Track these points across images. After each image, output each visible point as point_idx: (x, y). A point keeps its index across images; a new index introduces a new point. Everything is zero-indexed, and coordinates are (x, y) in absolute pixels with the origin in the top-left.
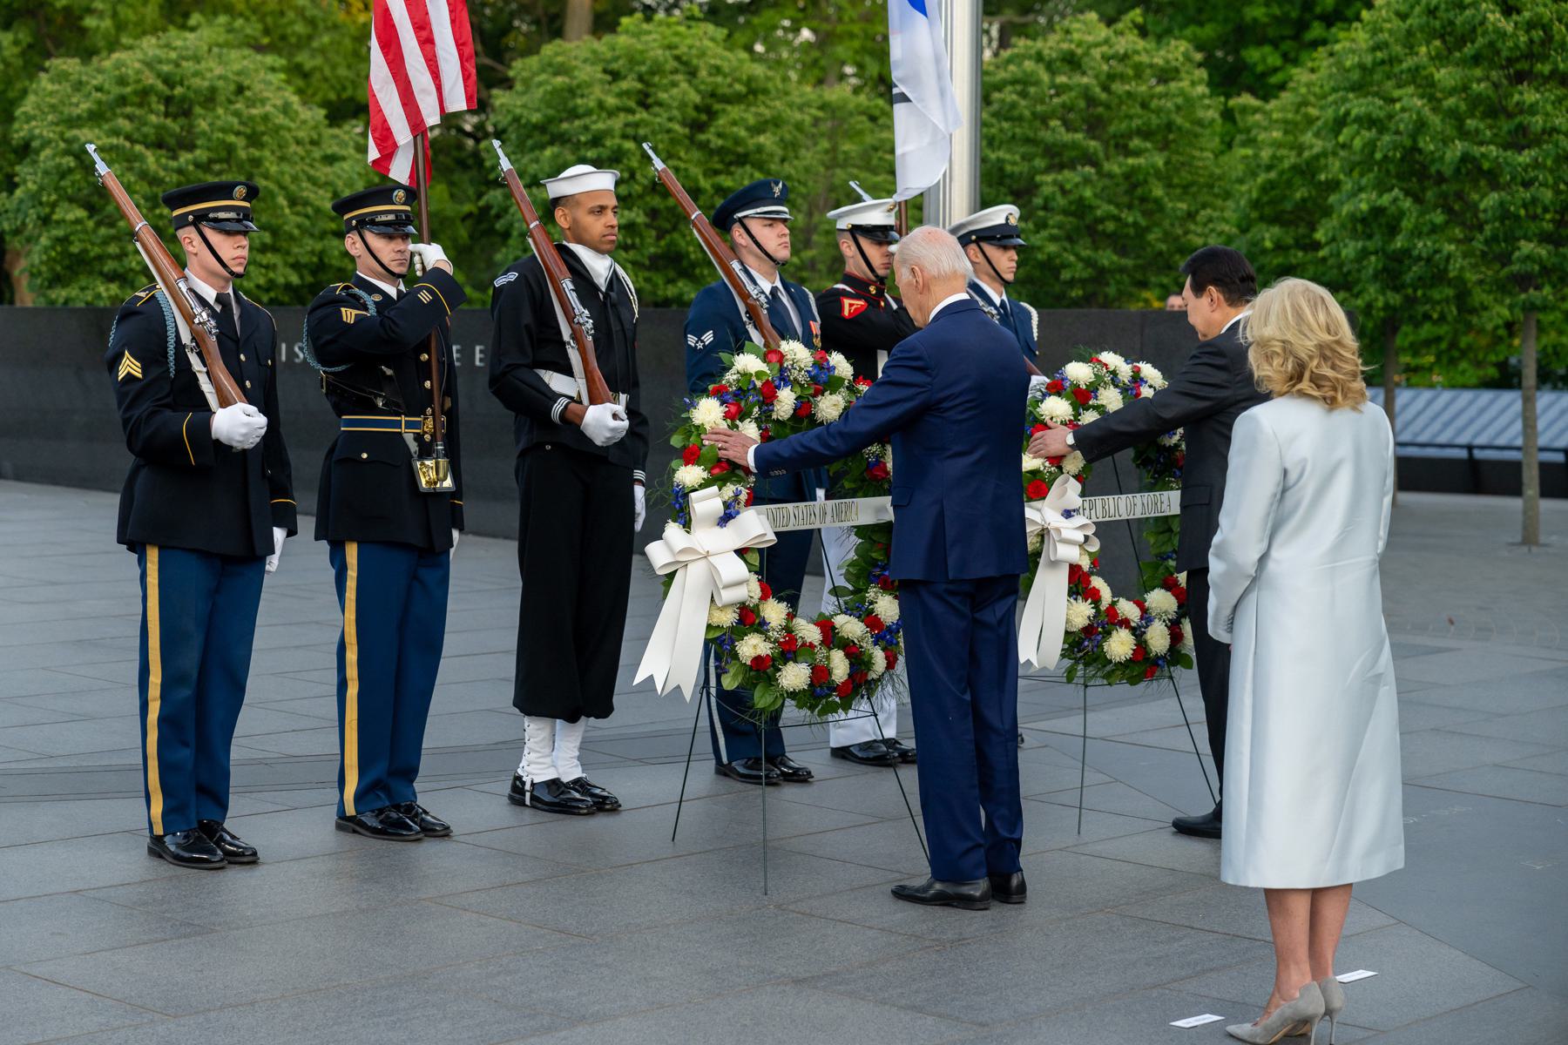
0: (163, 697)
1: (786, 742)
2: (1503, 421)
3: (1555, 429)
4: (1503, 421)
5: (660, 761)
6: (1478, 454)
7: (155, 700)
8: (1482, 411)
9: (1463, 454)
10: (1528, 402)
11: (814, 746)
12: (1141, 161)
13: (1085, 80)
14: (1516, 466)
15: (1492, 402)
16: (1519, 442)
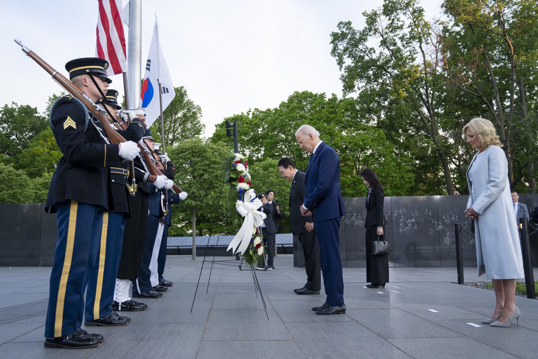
0: (71, 273)
1: (344, 281)
2: (198, 241)
3: (289, 236)
4: (198, 241)
5: (7, 309)
6: (179, 248)
7: (66, 273)
8: (173, 240)
9: (177, 248)
10: (193, 239)
11: (7, 309)
12: (16, 191)
13: (3, 175)
14: (191, 250)
15: (171, 239)
16: (191, 244)
